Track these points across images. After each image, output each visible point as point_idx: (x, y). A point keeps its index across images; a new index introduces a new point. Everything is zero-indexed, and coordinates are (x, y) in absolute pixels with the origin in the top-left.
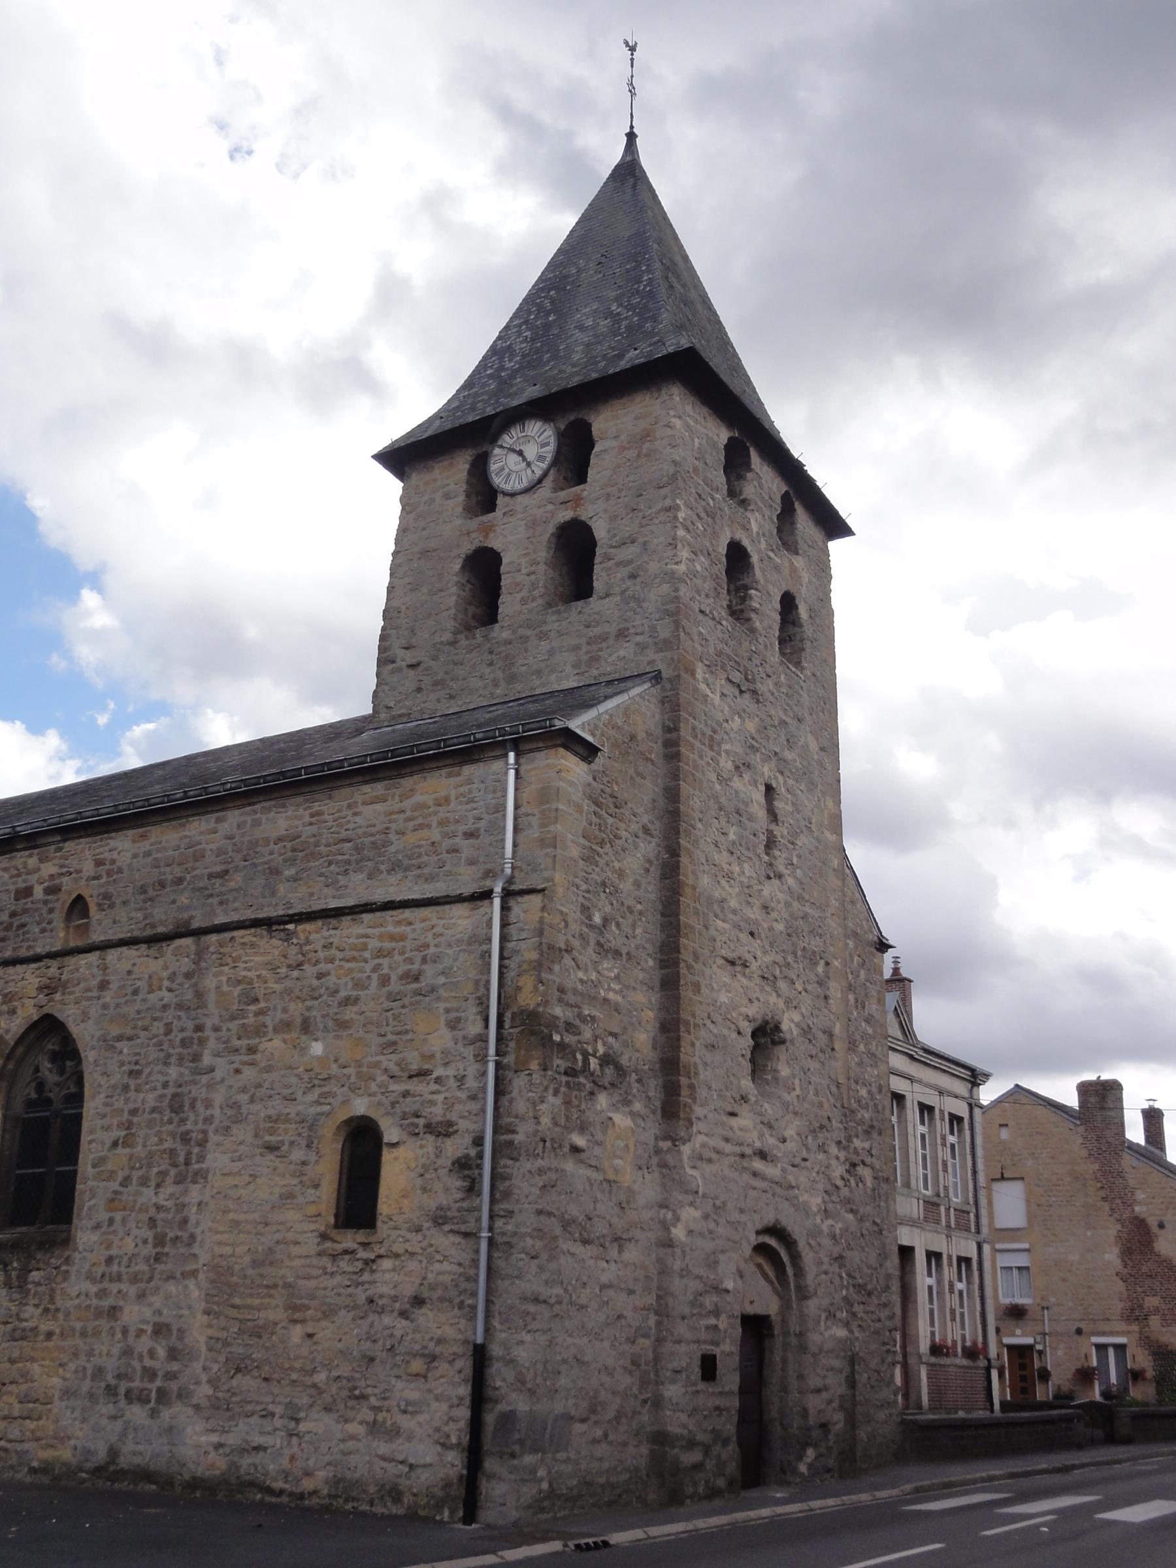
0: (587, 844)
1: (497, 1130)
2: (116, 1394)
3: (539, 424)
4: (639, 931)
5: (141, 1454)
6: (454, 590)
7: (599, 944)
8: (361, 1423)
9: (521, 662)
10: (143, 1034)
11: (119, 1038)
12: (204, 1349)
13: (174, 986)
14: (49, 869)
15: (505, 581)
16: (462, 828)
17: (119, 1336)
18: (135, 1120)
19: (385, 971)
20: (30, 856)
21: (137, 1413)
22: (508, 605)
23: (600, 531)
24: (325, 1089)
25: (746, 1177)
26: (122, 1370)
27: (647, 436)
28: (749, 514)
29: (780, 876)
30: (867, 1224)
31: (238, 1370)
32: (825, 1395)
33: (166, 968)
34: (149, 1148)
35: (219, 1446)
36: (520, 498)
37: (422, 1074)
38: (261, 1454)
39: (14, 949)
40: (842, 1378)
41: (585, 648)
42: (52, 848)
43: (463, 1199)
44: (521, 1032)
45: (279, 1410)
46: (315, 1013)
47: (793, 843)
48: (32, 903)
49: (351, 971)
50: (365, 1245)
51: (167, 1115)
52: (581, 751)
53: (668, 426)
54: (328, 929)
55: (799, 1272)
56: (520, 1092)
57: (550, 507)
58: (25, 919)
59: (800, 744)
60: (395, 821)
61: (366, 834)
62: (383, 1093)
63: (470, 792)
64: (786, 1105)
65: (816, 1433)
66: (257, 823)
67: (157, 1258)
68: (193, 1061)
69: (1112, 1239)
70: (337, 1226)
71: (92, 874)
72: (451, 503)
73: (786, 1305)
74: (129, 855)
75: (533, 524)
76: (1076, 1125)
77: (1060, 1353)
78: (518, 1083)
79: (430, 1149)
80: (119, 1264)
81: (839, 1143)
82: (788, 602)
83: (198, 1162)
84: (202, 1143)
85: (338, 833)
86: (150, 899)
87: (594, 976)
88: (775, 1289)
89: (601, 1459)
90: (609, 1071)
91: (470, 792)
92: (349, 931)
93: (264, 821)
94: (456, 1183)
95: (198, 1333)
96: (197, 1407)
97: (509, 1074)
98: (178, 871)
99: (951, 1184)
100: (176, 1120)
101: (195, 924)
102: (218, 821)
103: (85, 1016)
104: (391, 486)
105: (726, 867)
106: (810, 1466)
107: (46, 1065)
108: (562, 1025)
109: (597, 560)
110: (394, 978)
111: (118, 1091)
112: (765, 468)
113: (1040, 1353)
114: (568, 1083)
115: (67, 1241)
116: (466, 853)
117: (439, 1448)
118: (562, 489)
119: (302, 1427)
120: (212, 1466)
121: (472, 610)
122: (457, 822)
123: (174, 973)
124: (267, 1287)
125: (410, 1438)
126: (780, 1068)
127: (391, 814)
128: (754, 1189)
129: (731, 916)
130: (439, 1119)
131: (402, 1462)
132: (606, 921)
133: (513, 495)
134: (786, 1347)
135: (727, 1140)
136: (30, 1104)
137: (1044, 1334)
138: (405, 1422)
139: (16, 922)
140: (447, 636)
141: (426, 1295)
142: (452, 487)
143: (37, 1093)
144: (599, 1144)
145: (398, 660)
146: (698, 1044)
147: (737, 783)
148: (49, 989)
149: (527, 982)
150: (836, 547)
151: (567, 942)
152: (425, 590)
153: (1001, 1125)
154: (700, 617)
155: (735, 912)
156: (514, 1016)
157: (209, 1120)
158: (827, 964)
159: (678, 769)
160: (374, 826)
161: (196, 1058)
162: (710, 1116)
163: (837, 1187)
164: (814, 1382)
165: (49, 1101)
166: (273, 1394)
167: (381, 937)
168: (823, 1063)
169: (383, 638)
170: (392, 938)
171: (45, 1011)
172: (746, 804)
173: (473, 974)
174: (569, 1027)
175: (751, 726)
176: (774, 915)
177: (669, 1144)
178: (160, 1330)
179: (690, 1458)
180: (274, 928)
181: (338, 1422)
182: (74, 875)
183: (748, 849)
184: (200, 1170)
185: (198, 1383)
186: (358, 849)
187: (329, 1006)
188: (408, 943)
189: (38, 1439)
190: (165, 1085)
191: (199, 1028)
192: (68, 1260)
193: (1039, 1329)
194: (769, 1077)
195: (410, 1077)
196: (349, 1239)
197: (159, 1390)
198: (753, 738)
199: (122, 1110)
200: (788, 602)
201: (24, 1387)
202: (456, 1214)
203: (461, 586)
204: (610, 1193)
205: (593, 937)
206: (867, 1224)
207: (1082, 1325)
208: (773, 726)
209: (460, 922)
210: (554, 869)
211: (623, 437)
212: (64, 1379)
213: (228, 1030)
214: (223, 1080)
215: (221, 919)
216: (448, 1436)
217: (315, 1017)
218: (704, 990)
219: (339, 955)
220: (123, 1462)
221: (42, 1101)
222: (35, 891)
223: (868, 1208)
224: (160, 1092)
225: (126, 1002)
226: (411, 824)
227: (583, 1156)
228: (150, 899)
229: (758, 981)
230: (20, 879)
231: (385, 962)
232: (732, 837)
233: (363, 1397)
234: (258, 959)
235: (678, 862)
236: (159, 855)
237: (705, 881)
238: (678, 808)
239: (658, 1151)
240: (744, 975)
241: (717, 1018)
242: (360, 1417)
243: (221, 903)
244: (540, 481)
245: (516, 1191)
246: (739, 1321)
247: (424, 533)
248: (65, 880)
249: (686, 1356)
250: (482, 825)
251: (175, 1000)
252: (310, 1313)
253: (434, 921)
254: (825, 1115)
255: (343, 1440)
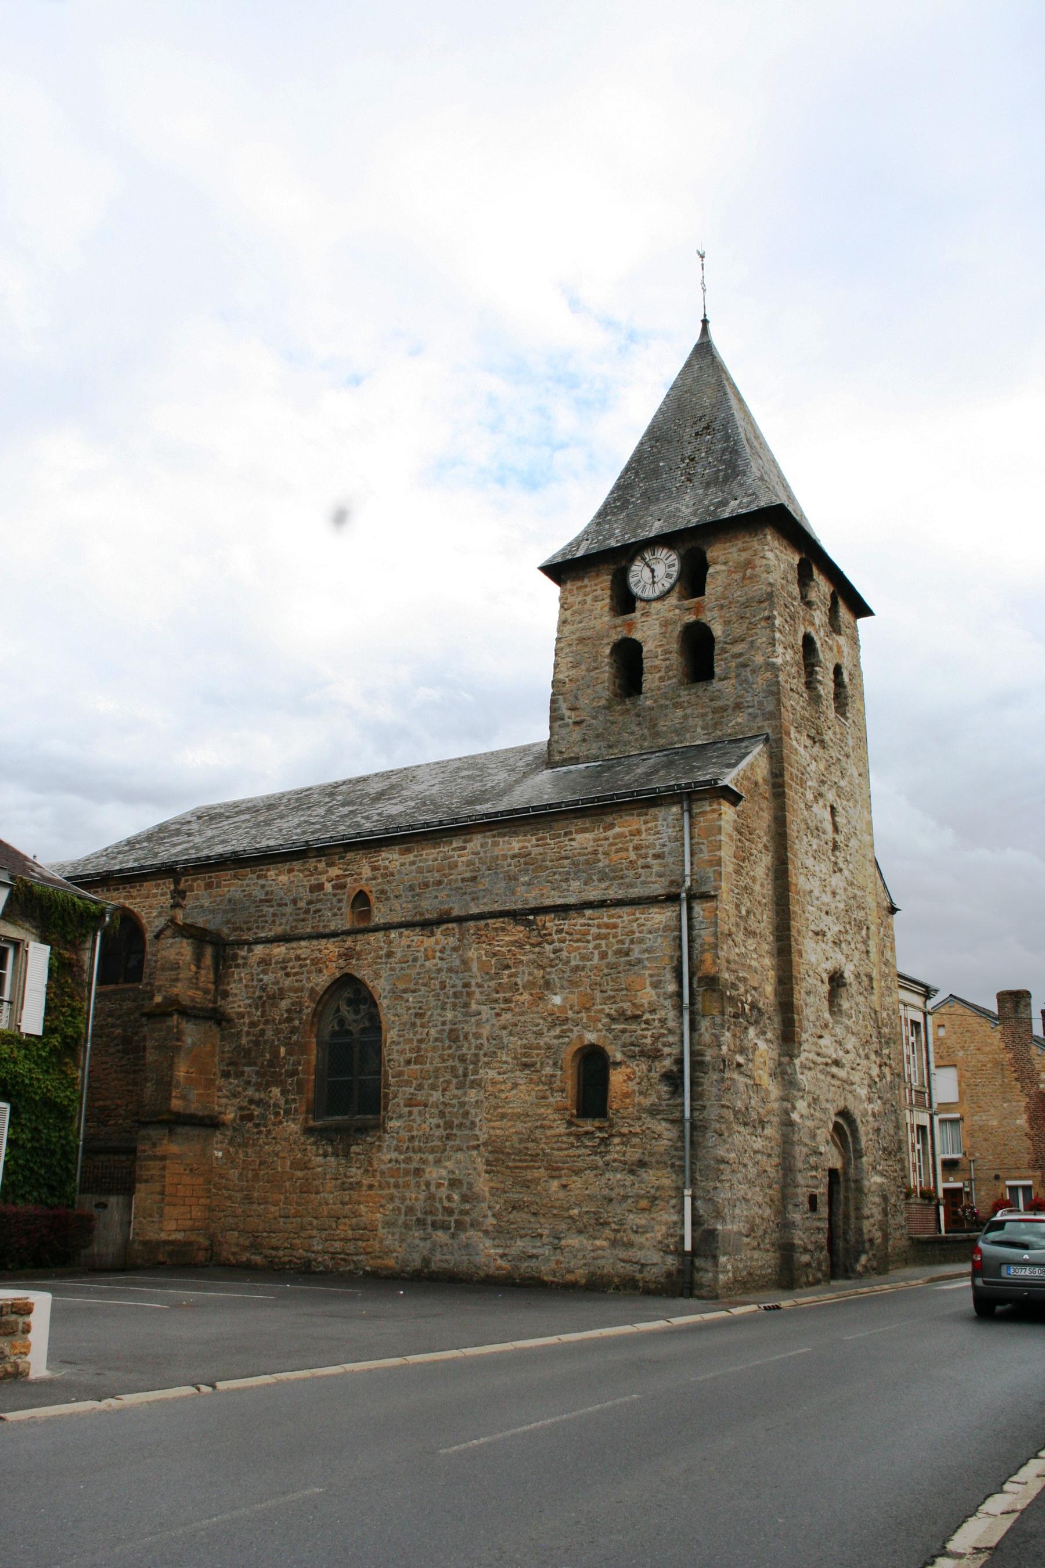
0: (737, 861)
1: (692, 1053)
2: (425, 1224)
3: (665, 551)
4: (765, 917)
5: (447, 1261)
6: (607, 668)
7: (745, 929)
8: (605, 1240)
9: (662, 723)
10: (423, 988)
11: (405, 991)
12: (487, 1194)
13: (445, 956)
14: (334, 872)
15: (647, 664)
16: (651, 852)
17: (424, 1188)
18: (423, 1046)
19: (604, 948)
20: (320, 861)
21: (441, 1236)
22: (650, 681)
23: (717, 630)
24: (565, 1027)
25: (829, 1078)
26: (428, 1209)
27: (748, 564)
28: (813, 613)
29: (841, 870)
30: (888, 1106)
31: (514, 1208)
32: (872, 1220)
33: (437, 943)
34: (435, 1065)
35: (502, 1256)
36: (654, 604)
37: (636, 1018)
38: (534, 1260)
39: (313, 927)
40: (880, 1208)
41: (710, 716)
42: (337, 857)
43: (669, 1099)
44: (706, 990)
45: (546, 1232)
46: (553, 976)
47: (847, 846)
48: (324, 895)
49: (578, 948)
50: (600, 1129)
51: (447, 1043)
52: (732, 798)
53: (763, 557)
54: (559, 920)
55: (856, 1140)
56: (707, 1029)
57: (677, 611)
58: (319, 906)
59: (848, 774)
60: (601, 846)
61: (580, 854)
62: (607, 1030)
63: (656, 826)
64: (847, 1028)
65: (867, 1245)
66: (495, 844)
67: (448, 1137)
68: (463, 1007)
69: (1023, 1109)
70: (579, 1116)
71: (370, 875)
72: (599, 604)
73: (846, 1163)
74: (398, 864)
75: (665, 624)
76: (996, 1025)
77: (983, 1193)
78: (704, 1024)
79: (644, 1067)
80: (419, 1141)
81: (876, 1052)
82: (838, 670)
83: (473, 1075)
84: (475, 1063)
85: (559, 853)
86: (417, 895)
87: (743, 950)
88: (840, 1152)
89: (757, 1260)
90: (755, 1013)
91: (656, 826)
92: (577, 922)
93: (501, 843)
94: (664, 1088)
95: (482, 1185)
96: (486, 1232)
97: (698, 1018)
98: (437, 876)
99: (912, 1073)
100: (454, 1046)
101: (455, 913)
102: (465, 841)
103: (377, 976)
104: (552, 590)
105: (812, 868)
106: (865, 1266)
107: (344, 1008)
108: (729, 985)
109: (717, 651)
110: (610, 953)
111: (408, 1026)
112: (821, 577)
113: (968, 1193)
114: (734, 1022)
115: (379, 1126)
116: (656, 869)
117: (662, 1253)
118: (686, 599)
119: (563, 1242)
120: (499, 1268)
121: (617, 681)
122: (647, 847)
123: (444, 948)
124: (531, 1155)
125: (641, 1248)
126: (842, 1003)
127: (599, 840)
128: (834, 1086)
129: (815, 902)
130: (649, 1047)
131: (636, 1263)
132: (748, 912)
133: (648, 601)
134: (847, 1189)
135: (818, 1054)
136: (334, 1034)
137: (970, 1180)
138: (638, 1239)
139: (312, 907)
140: (603, 702)
141: (646, 1159)
142: (599, 592)
143: (338, 1026)
144: (751, 1061)
145: (566, 718)
146: (802, 991)
147: (816, 808)
148: (347, 955)
149: (708, 957)
150: (861, 622)
151: (729, 930)
152: (583, 667)
153: (939, 1026)
154: (791, 694)
155: (818, 899)
156: (699, 978)
157: (479, 1047)
158: (868, 928)
159: (784, 803)
160: (586, 848)
161: (466, 1005)
162: (810, 1039)
163: (876, 1083)
164: (866, 1212)
165: (349, 1033)
166: (540, 1223)
167: (599, 926)
168: (866, 998)
169: (553, 701)
170: (607, 926)
171: (346, 971)
172: (821, 822)
173: (669, 952)
174: (734, 986)
175: (822, 766)
176: (838, 898)
177: (787, 1059)
178: (454, 1183)
179: (805, 1258)
180: (518, 918)
181: (588, 1239)
182: (355, 877)
183: (823, 854)
184: (475, 1080)
185: (485, 1216)
186: (575, 864)
187: (563, 972)
188: (619, 930)
189: (368, 1253)
190: (444, 1023)
191: (466, 985)
192: (380, 1139)
193: (967, 1176)
194: (836, 1009)
195: (626, 1019)
196: (589, 1125)
197: (456, 1221)
198: (823, 775)
199: (412, 1039)
200: (838, 670)
201: (354, 1220)
202: (665, 1108)
203: (611, 665)
204: (757, 1092)
205: (742, 924)
206: (888, 1106)
207: (999, 1173)
208: (833, 764)
209: (656, 916)
210: (721, 881)
211: (731, 564)
212: (385, 1215)
213: (489, 987)
214: (487, 1020)
215: (474, 910)
216: (668, 1246)
217: (553, 979)
218: (804, 955)
219: (568, 937)
220: (433, 1267)
221: (342, 1031)
222: (325, 887)
223: (889, 1095)
224: (440, 1028)
225: (408, 966)
226: (613, 848)
227: (742, 1069)
228: (417, 895)
229: (831, 944)
230: (312, 878)
231: (603, 942)
232: (815, 847)
233: (606, 1224)
234: (507, 939)
235: (787, 869)
236: (422, 864)
237: (802, 879)
238: (785, 831)
239: (780, 1064)
240: (823, 941)
241: (811, 973)
242: (604, 1236)
243: (473, 899)
244: (669, 591)
245: (707, 1093)
246: (827, 1173)
247: (580, 625)
248: (349, 880)
249: (802, 1195)
250: (666, 849)
251: (446, 966)
252: (563, 1172)
253: (638, 916)
254: (869, 1033)
255: (593, 1251)
